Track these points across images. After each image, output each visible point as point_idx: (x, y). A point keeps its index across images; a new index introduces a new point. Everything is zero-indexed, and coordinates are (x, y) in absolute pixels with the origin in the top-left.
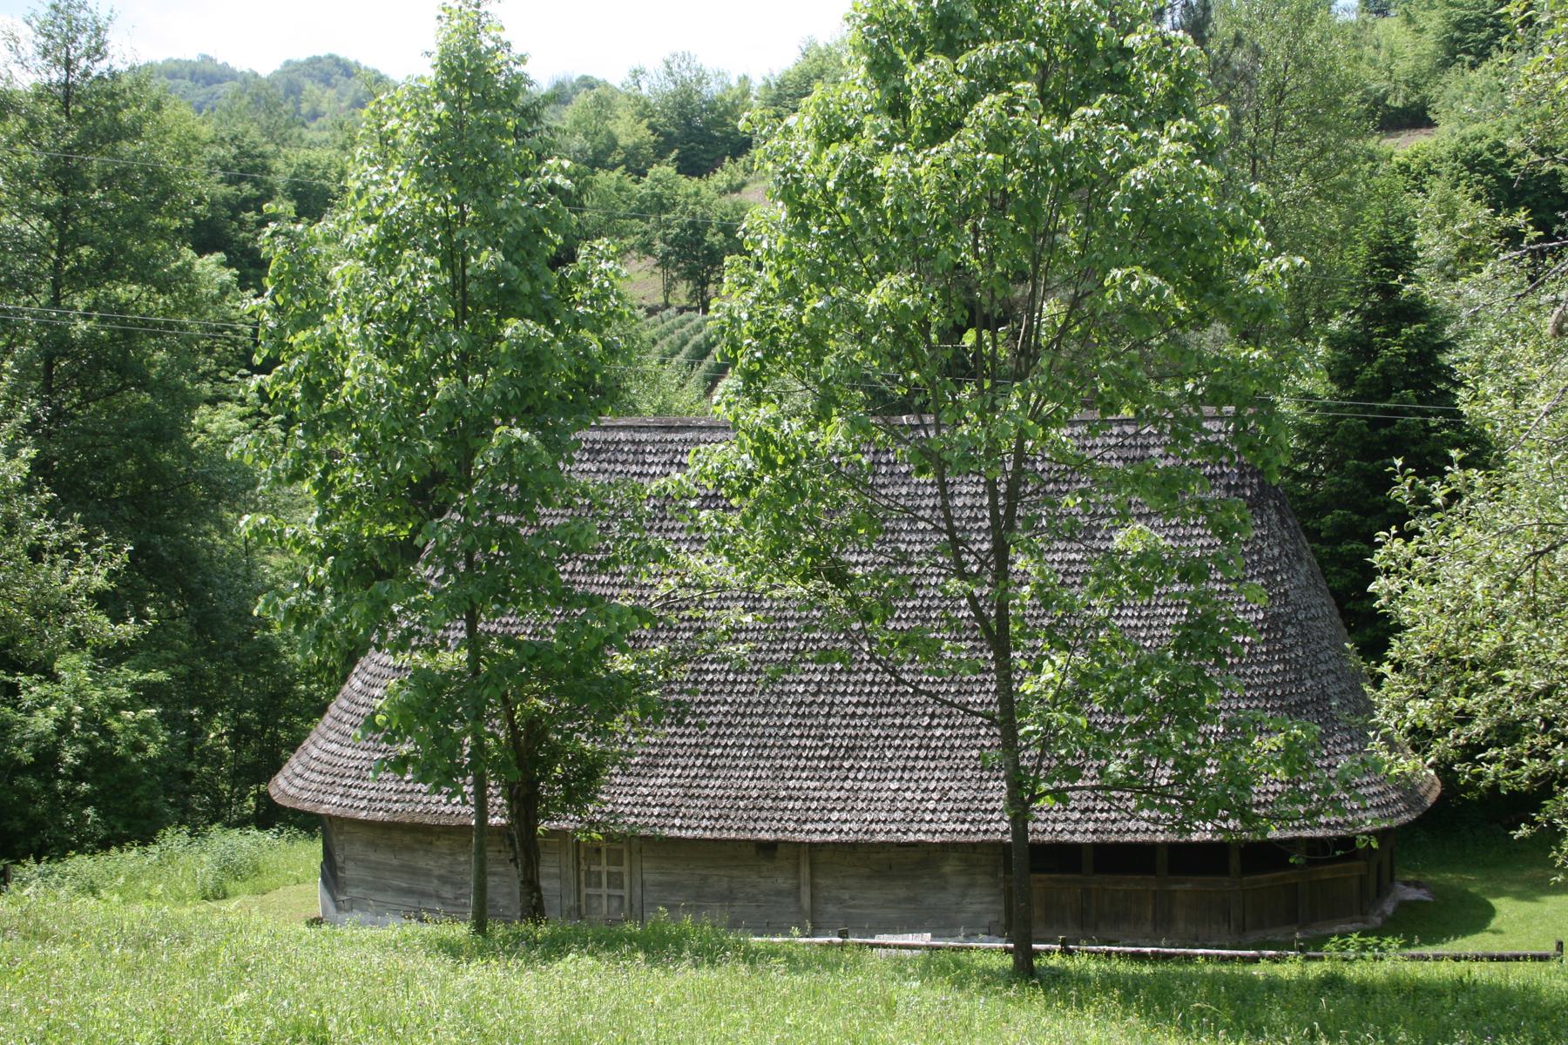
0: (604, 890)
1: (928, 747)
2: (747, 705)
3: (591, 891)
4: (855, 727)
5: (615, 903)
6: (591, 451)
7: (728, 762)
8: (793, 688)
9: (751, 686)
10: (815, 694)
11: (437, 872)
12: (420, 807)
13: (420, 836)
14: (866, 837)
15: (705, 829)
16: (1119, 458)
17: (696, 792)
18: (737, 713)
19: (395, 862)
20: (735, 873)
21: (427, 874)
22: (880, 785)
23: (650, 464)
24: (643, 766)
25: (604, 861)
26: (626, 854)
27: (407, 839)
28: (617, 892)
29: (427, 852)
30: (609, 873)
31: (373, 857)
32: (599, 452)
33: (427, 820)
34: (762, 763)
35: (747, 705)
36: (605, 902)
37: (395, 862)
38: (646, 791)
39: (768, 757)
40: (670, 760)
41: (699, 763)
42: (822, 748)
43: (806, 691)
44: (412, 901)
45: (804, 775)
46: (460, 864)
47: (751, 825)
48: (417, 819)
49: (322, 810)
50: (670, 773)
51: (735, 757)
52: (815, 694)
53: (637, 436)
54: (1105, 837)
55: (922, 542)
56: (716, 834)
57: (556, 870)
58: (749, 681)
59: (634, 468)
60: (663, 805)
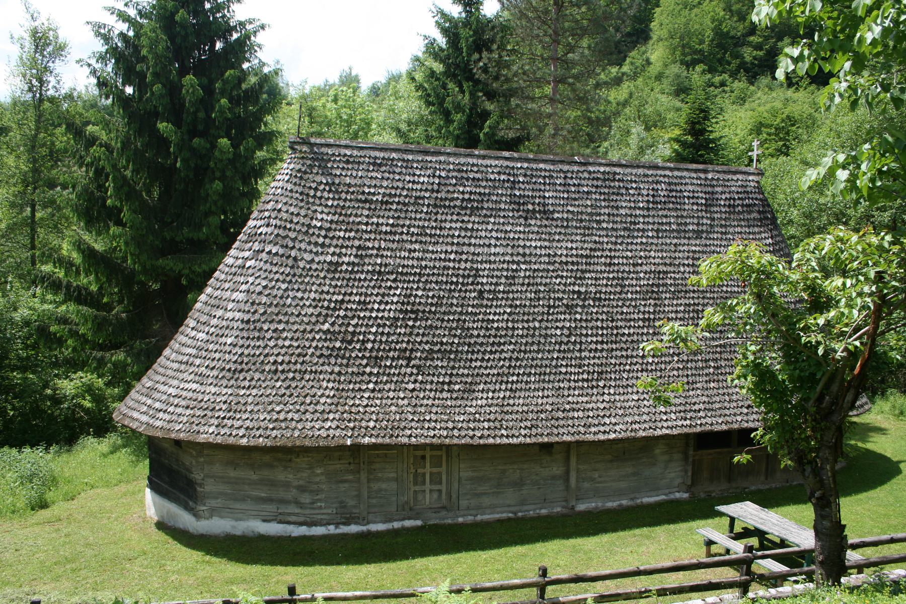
1: (589, 373)
2: (526, 345)
3: (417, 488)
4: (599, 358)
5: (435, 496)
6: (374, 164)
7: (523, 386)
8: (553, 331)
9: (525, 332)
10: (569, 336)
11: (296, 483)
12: (297, 433)
13: (280, 455)
14: (633, 434)
15: (525, 436)
17: (509, 409)
18: (520, 351)
19: (255, 477)
20: (525, 466)
21: (287, 485)
22: (626, 397)
23: (419, 176)
24: (464, 391)
25: (428, 465)
26: (444, 458)
27: (267, 458)
28: (437, 487)
29: (286, 468)
30: (431, 474)
31: (232, 473)
32: (380, 165)
33: (307, 443)
34: (546, 386)
35: (526, 345)
36: (428, 496)
37: (255, 477)
38: (473, 410)
40: (481, 387)
41: (503, 387)
42: (582, 373)
43: (562, 334)
44: (271, 508)
45: (576, 393)
46: (318, 475)
47: (555, 431)
48: (298, 443)
49: (202, 438)
50: (485, 396)
51: (527, 383)
52: (569, 336)
53: (406, 157)
54: (731, 426)
55: (607, 236)
56: (534, 440)
57: (393, 475)
58: (523, 328)
59: (408, 178)
60: (489, 420)
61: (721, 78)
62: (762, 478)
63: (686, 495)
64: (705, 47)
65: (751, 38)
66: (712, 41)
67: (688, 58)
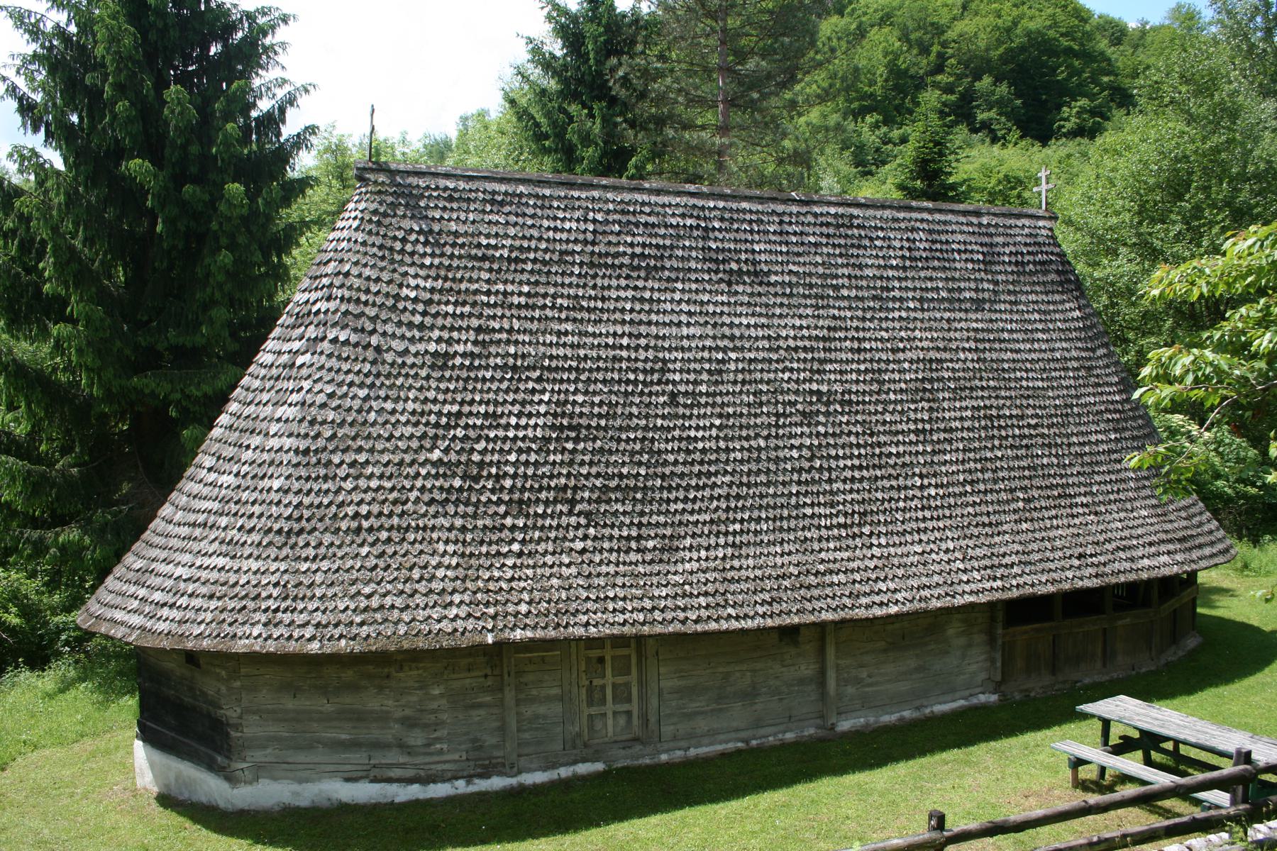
0: (610, 706)
3: (594, 710)
5: (622, 721)
7: (751, 538)
10: (810, 459)
11: (399, 714)
12: (402, 629)
14: (923, 605)
16: (927, 240)
19: (329, 708)
21: (383, 718)
25: (609, 672)
27: (348, 675)
28: (625, 707)
29: (381, 689)
30: (614, 685)
31: (290, 704)
32: (502, 204)
33: (421, 644)
36: (610, 722)
37: (329, 708)
39: (789, 529)
46: (434, 698)
48: (406, 645)
49: (241, 646)
54: (1061, 586)
57: (555, 691)
58: (742, 449)
61: (901, 131)
62: (1099, 664)
63: (994, 698)
64: (878, 89)
65: (939, 78)
66: (886, 81)
67: (855, 105)
